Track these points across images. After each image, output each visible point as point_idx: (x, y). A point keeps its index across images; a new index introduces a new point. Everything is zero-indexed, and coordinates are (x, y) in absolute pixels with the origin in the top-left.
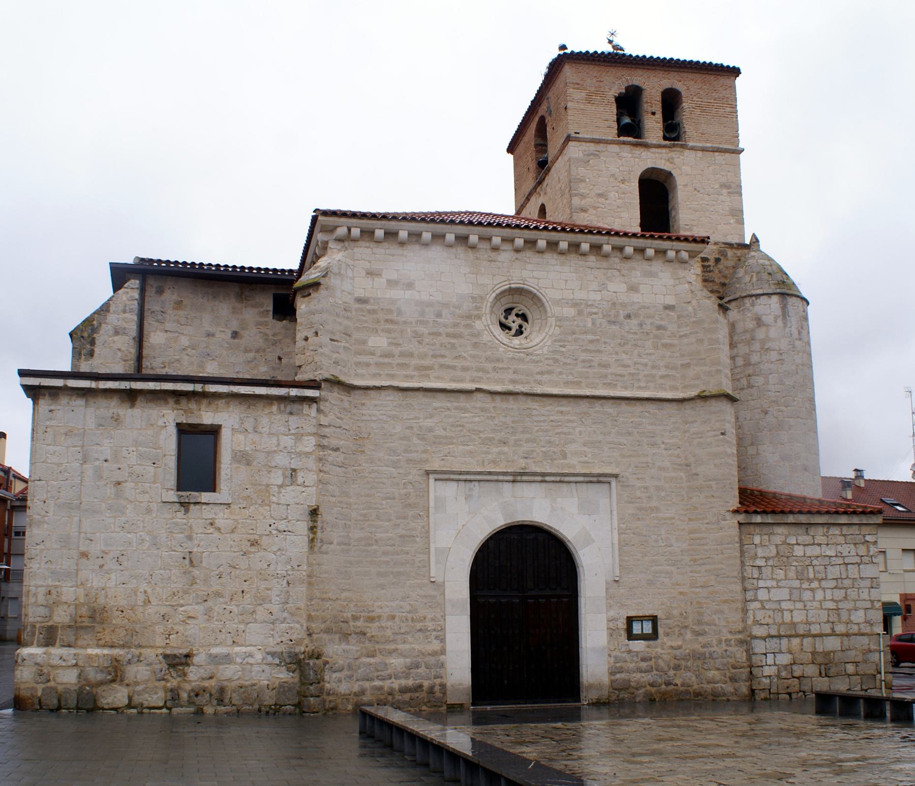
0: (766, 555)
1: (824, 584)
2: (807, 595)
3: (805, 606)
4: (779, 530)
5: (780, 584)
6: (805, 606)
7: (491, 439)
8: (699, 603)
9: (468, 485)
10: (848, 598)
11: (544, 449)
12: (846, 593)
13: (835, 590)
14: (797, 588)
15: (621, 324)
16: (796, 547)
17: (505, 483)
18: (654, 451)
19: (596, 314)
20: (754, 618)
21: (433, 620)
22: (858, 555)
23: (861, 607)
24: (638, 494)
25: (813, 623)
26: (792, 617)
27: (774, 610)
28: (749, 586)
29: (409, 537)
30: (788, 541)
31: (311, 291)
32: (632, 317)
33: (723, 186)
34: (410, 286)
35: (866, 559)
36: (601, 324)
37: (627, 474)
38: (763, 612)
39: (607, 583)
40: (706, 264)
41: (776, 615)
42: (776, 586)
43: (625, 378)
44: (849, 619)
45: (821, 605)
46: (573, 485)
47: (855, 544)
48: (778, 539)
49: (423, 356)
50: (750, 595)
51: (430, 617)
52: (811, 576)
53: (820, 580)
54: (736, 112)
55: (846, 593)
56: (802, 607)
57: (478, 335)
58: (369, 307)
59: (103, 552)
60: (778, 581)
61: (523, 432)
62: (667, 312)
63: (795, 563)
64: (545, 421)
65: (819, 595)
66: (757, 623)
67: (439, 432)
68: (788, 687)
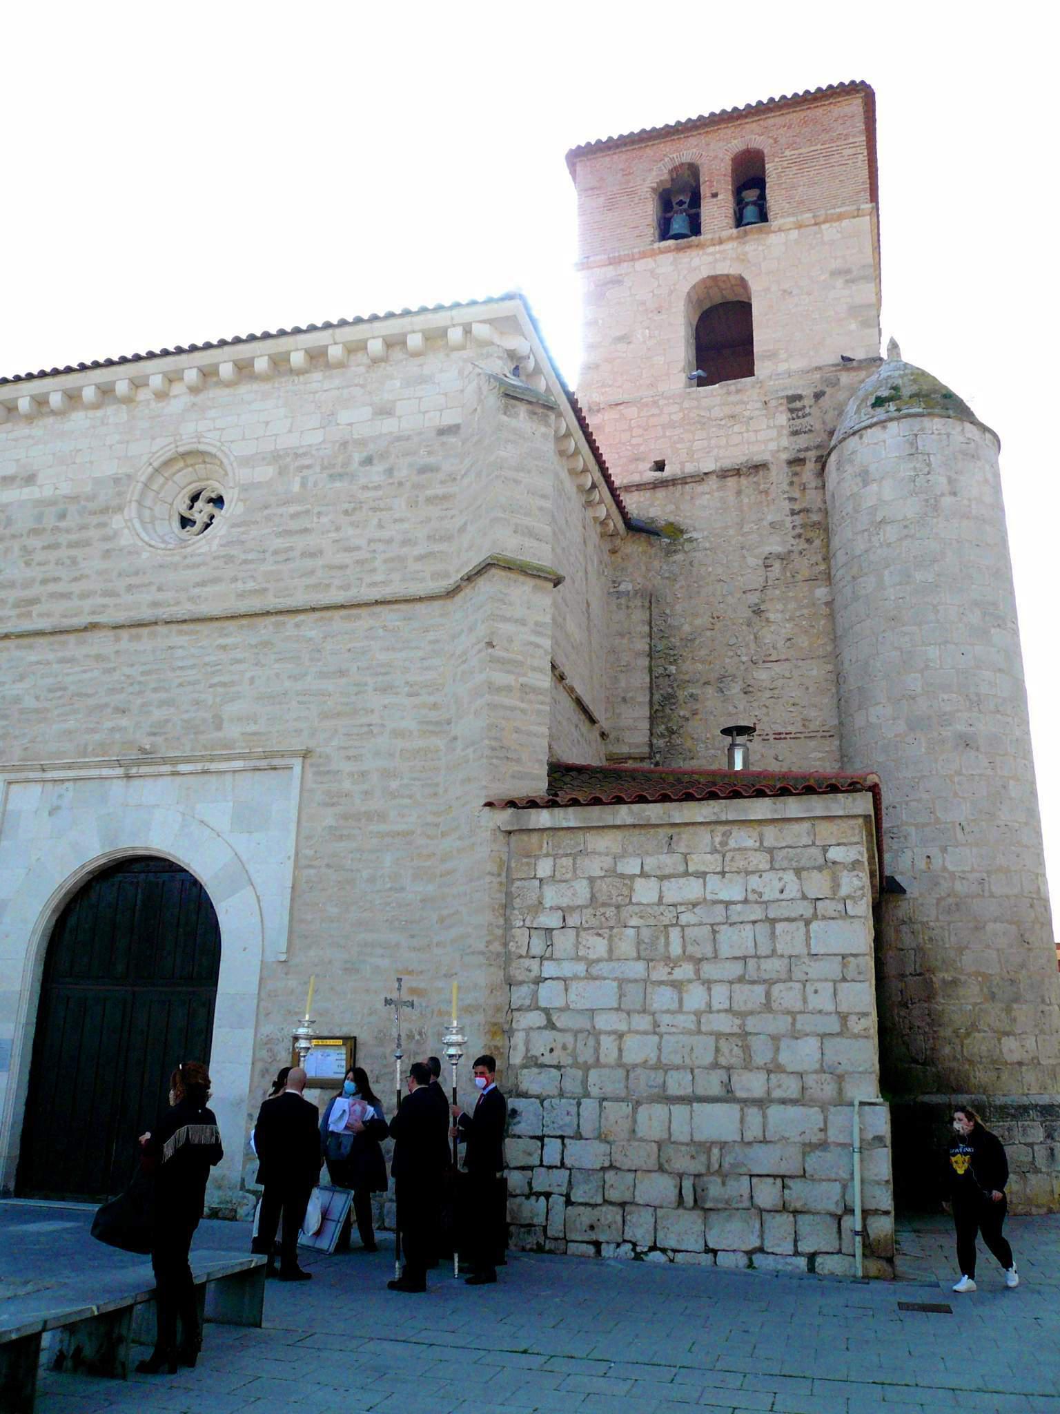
0: (564, 902)
1: (708, 970)
2: (663, 998)
3: (656, 1025)
4: (603, 843)
5: (595, 971)
6: (656, 1025)
7: (102, 707)
9: (60, 788)
10: (775, 1006)
11: (186, 716)
12: (768, 995)
13: (736, 986)
14: (636, 981)
15: (352, 477)
16: (639, 884)
18: (386, 702)
19: (308, 467)
20: (527, 1050)
22: (804, 897)
23: (808, 1029)
24: (347, 785)
25: (677, 1068)
26: (620, 1050)
27: (576, 1033)
28: (518, 974)
30: (620, 870)
32: (375, 461)
33: (836, 273)
34: (30, 479)
35: (827, 907)
36: (315, 484)
38: (549, 1035)
40: (798, 404)
41: (580, 1045)
42: (583, 974)
43: (348, 572)
44: (774, 1060)
45: (699, 1022)
47: (798, 872)
48: (595, 867)
49: (27, 584)
50: (520, 995)
52: (676, 949)
53: (698, 961)
55: (768, 995)
56: (649, 1027)
57: (115, 535)
60: (590, 963)
61: (155, 690)
62: (444, 438)
63: (634, 921)
64: (193, 667)
65: (695, 997)
66: (533, 1062)
67: (30, 703)
68: (592, 1227)
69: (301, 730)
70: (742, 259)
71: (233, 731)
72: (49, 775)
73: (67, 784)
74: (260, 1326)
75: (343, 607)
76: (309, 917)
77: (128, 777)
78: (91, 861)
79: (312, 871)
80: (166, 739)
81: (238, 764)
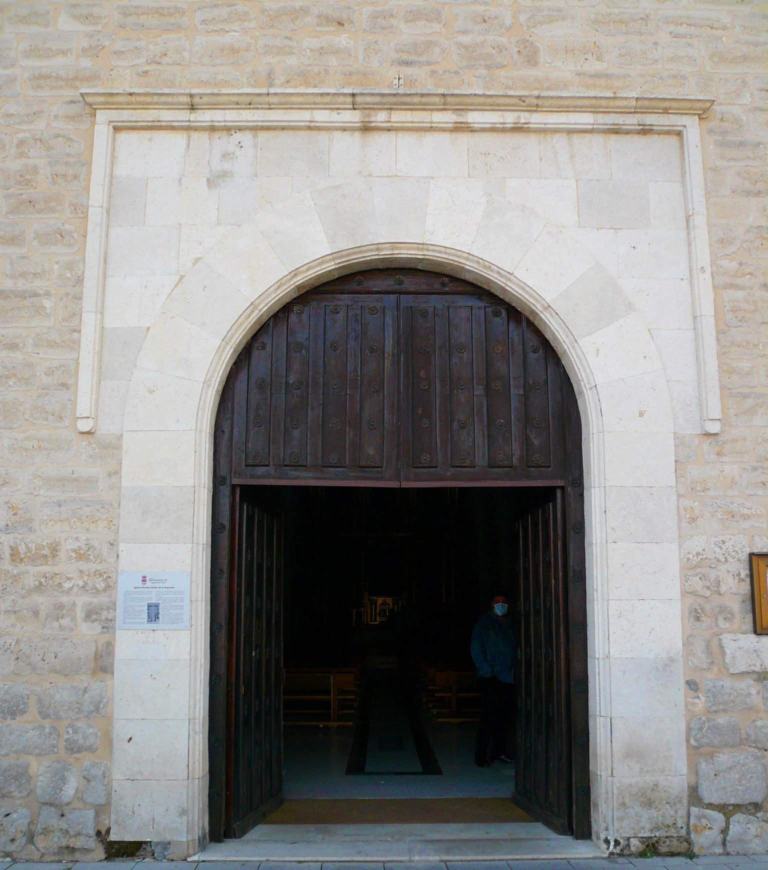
9: (222, 143)
11: (466, 39)
17: (338, 135)
21: (81, 556)
29: (23, 295)
37: (737, 110)
39: (680, 441)
46: (560, 141)
51: (70, 545)
69: (684, 77)
72: (205, 117)
73: (238, 136)
76: (745, 365)
77: (366, 128)
78: (309, 266)
79: (740, 294)
80: (433, 72)
81: (586, 119)
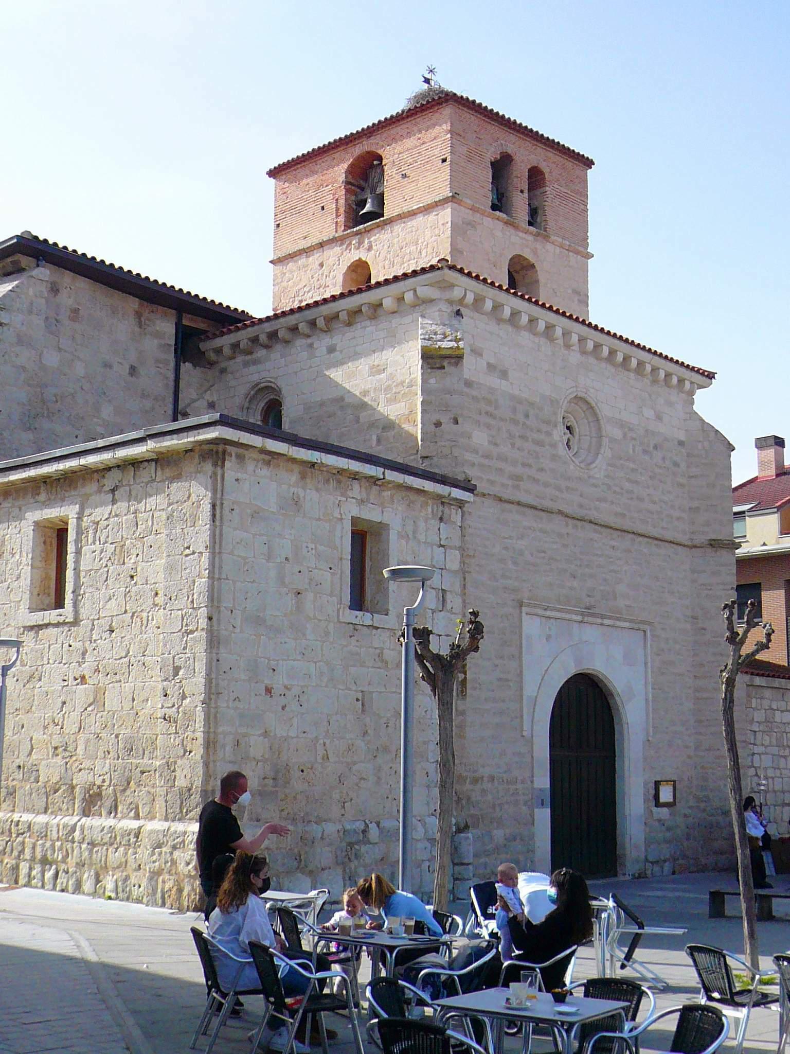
8: (702, 767)
31: (445, 364)
34: (504, 374)
54: (586, 211)
58: (475, 393)
59: (286, 687)
70: (535, 251)
71: (621, 603)
72: (548, 613)
74: (711, 894)
75: (656, 539)
81: (627, 624)
